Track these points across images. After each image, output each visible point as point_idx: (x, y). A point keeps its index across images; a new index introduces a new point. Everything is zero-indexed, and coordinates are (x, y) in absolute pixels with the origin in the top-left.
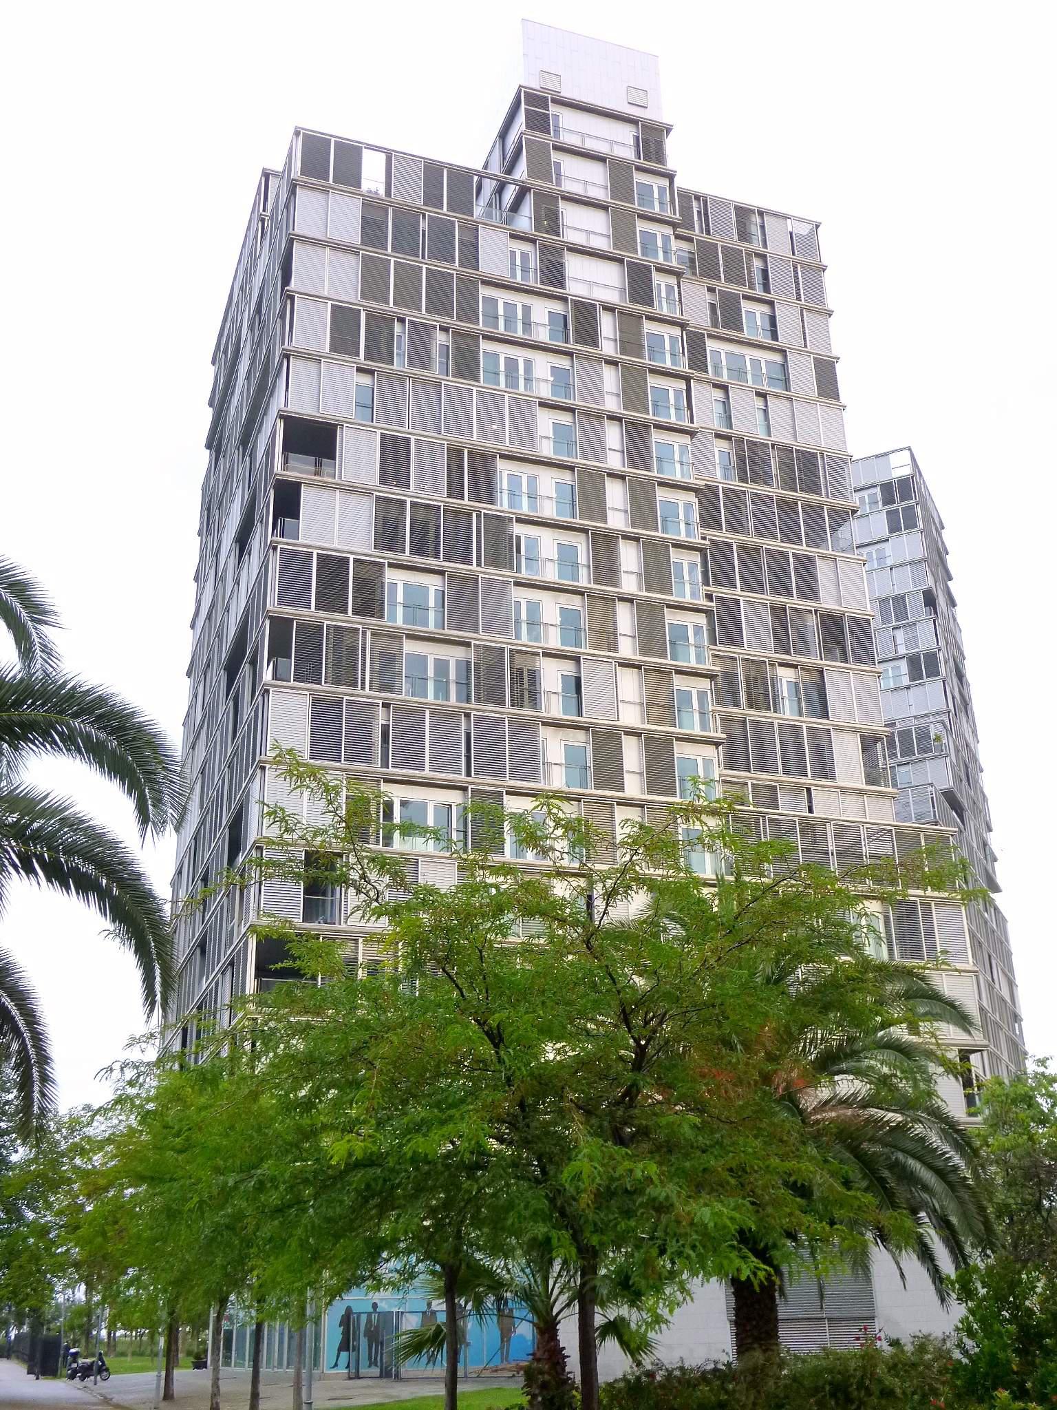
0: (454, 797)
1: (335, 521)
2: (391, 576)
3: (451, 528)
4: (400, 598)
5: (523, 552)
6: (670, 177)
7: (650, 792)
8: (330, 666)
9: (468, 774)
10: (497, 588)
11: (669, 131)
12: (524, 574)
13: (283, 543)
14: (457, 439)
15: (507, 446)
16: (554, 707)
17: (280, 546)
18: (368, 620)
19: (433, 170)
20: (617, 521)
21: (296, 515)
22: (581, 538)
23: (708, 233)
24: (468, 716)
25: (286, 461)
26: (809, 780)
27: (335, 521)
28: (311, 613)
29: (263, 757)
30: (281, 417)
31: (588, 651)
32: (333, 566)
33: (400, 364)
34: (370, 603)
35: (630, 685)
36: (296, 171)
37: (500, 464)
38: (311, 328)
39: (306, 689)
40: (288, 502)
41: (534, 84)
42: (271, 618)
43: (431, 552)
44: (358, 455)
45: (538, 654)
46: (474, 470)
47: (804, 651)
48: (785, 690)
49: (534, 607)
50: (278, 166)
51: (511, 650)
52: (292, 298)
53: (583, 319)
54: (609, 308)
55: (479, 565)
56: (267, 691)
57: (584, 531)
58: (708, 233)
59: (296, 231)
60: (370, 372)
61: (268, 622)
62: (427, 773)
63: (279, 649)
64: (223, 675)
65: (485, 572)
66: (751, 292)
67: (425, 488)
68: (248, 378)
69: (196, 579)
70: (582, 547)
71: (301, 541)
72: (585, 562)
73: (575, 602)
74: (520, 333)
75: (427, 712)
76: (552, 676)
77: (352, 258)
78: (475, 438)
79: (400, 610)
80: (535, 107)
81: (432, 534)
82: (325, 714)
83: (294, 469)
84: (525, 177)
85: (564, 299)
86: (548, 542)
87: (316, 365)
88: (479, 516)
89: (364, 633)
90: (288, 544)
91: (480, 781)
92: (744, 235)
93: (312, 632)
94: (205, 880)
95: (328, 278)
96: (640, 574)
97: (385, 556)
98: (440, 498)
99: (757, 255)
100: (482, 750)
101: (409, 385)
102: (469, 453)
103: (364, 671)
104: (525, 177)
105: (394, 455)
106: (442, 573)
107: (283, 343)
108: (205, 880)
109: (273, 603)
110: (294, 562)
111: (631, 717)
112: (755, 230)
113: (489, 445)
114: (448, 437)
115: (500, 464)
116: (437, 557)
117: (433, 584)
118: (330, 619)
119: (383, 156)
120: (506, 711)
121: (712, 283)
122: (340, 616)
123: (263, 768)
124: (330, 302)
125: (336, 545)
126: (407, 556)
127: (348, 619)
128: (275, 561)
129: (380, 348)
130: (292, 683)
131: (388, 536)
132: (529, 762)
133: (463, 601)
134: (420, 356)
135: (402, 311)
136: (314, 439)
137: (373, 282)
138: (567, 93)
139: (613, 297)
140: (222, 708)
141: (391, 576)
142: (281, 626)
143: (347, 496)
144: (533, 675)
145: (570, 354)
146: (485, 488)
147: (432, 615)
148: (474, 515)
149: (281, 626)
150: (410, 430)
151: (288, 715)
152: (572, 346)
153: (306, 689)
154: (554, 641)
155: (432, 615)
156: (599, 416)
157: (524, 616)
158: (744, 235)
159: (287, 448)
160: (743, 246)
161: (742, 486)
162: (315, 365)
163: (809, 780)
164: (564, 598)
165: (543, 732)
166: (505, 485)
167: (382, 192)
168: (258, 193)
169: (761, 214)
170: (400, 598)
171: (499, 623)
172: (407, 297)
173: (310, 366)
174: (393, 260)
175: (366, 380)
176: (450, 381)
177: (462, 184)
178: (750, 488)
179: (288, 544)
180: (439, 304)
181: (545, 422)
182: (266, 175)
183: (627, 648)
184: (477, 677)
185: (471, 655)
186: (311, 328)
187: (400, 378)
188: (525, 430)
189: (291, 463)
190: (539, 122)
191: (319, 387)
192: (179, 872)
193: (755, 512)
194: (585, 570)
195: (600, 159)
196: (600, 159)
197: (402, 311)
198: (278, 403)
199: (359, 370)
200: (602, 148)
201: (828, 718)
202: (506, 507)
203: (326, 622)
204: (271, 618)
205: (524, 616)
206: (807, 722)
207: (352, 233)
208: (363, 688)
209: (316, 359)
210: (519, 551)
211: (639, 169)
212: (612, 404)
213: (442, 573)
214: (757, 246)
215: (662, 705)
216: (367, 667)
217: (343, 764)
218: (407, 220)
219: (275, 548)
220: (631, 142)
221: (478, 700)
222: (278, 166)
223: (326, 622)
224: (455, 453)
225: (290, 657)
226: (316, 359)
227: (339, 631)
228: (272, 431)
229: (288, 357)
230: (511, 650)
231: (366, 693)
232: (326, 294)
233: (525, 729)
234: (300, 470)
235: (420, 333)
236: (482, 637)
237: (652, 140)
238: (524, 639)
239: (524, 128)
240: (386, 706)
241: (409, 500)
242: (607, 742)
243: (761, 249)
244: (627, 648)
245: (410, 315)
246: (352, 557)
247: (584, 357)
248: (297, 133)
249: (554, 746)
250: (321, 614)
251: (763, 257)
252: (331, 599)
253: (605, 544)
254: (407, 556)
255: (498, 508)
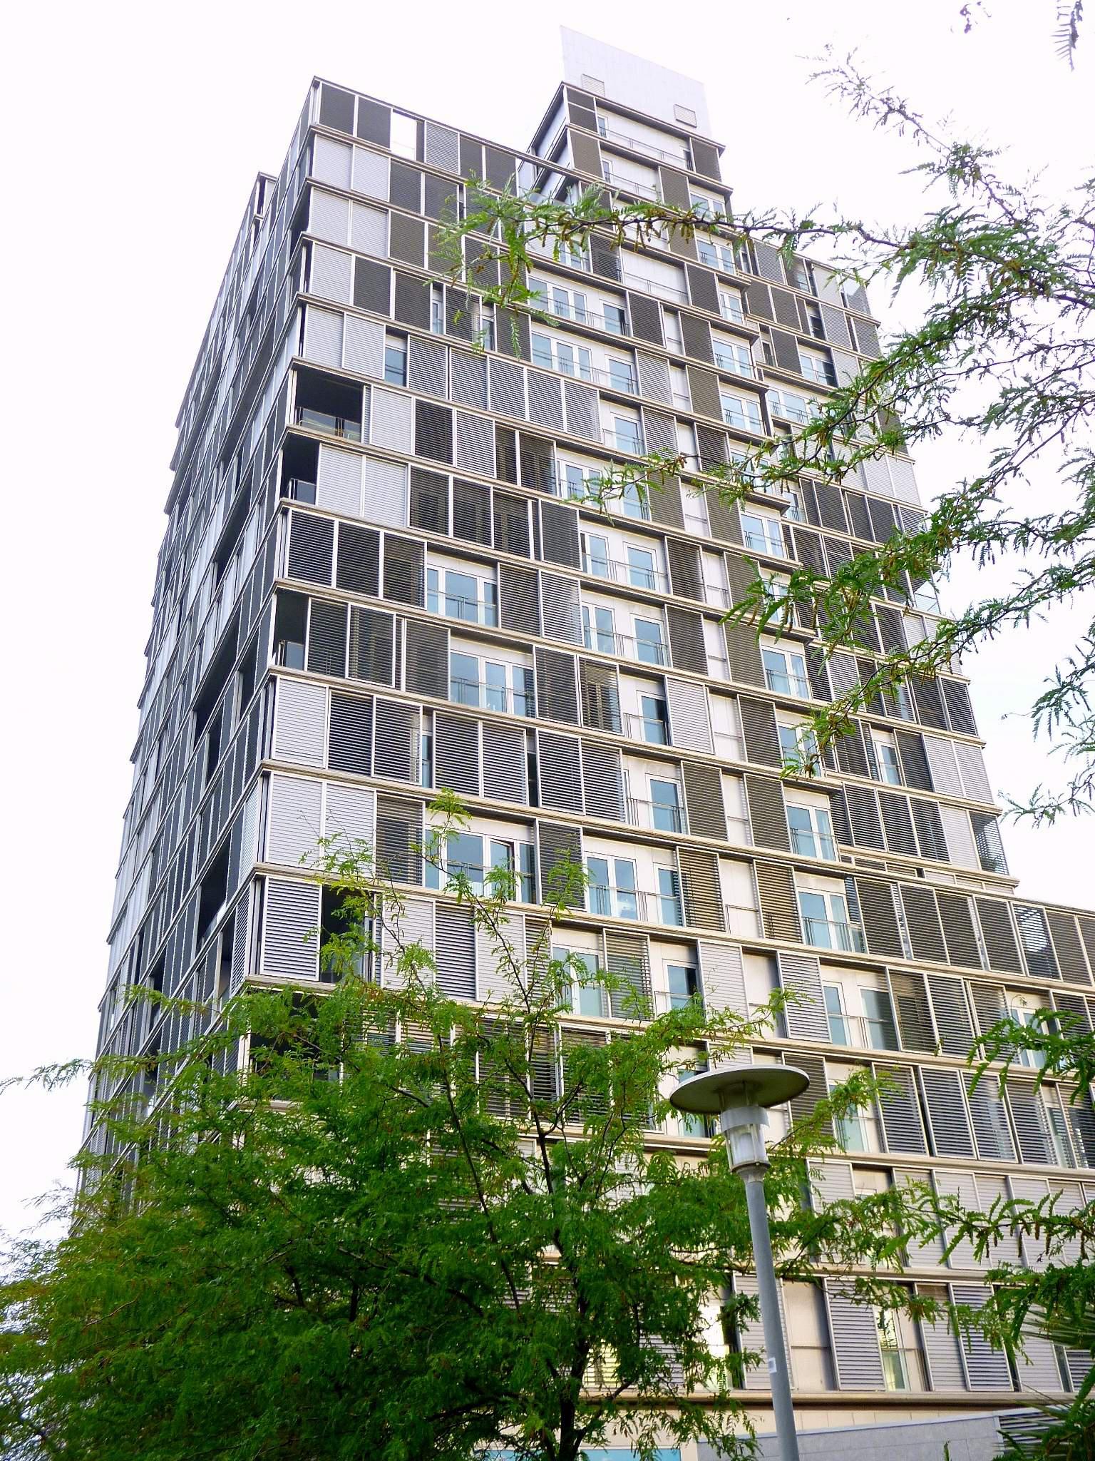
0: (517, 834)
1: (361, 488)
2: (431, 561)
3: (502, 508)
4: (442, 587)
5: (588, 551)
6: (726, 194)
7: (757, 844)
8: (356, 649)
9: (534, 802)
10: (559, 587)
11: (721, 150)
12: (591, 574)
13: (295, 506)
14: (509, 419)
15: (565, 432)
16: (638, 732)
17: (291, 509)
18: (403, 606)
19: (471, 145)
20: (695, 527)
21: (312, 478)
22: (653, 546)
23: (756, 273)
24: (531, 732)
25: (299, 417)
26: (919, 859)
27: (361, 488)
28: (332, 590)
29: (266, 761)
30: (294, 369)
31: (672, 669)
32: (359, 542)
33: (437, 328)
34: (406, 586)
35: (724, 715)
36: (315, 118)
37: (558, 455)
38: (332, 277)
39: (326, 681)
40: (301, 462)
41: (576, 82)
42: (280, 593)
43: (479, 532)
44: (390, 419)
45: (613, 668)
46: (530, 456)
47: (895, 713)
48: (881, 756)
49: (604, 614)
50: (275, 171)
51: (581, 659)
52: (308, 246)
53: (644, 315)
54: (672, 310)
55: (538, 557)
56: (273, 679)
57: (660, 536)
58: (756, 273)
59: (314, 176)
60: (402, 335)
61: (274, 598)
62: (481, 798)
63: (289, 629)
64: (192, 718)
65: (546, 567)
66: (805, 337)
67: (473, 466)
68: (234, 385)
69: (147, 653)
70: (657, 557)
71: (317, 505)
72: (661, 570)
73: (653, 614)
74: (572, 317)
75: (480, 724)
76: (632, 697)
77: (377, 217)
78: (526, 420)
79: (442, 601)
80: (580, 105)
81: (479, 522)
82: (349, 719)
83: (308, 425)
84: (572, 167)
85: (620, 293)
86: (617, 545)
87: (337, 319)
88: (535, 505)
89: (399, 622)
90: (302, 507)
91: (545, 813)
92: (793, 282)
93: (332, 615)
94: (157, 976)
95: (350, 234)
96: (725, 592)
97: (425, 536)
98: (489, 479)
99: (810, 303)
100: (549, 774)
101: (448, 357)
102: (521, 435)
103: (399, 660)
104: (572, 167)
105: (433, 429)
106: (492, 563)
107: (296, 287)
108: (157, 976)
109: (281, 572)
110: (311, 534)
111: (728, 751)
112: (802, 278)
113: (544, 429)
114: (493, 416)
115: (558, 455)
116: (487, 542)
117: (483, 575)
118: (355, 600)
119: (414, 123)
120: (578, 730)
121: (766, 322)
122: (371, 599)
123: (266, 776)
124: (354, 255)
125: (362, 516)
126: (449, 538)
127: (379, 602)
128: (284, 530)
129: (413, 302)
130: (306, 672)
131: (426, 509)
132: (607, 797)
133: (521, 600)
134: (461, 327)
135: (437, 276)
136: (335, 397)
137: (405, 239)
138: (613, 96)
139: (675, 299)
140: (189, 753)
141: (431, 561)
142: (292, 604)
143: (376, 464)
144: (607, 694)
145: (630, 349)
146: (540, 475)
147: (481, 611)
148: (530, 502)
149: (292, 604)
150: (450, 401)
151: (299, 710)
152: (631, 338)
153: (326, 681)
154: (631, 654)
155: (481, 611)
156: (666, 416)
157: (593, 624)
158: (793, 282)
159: (301, 402)
160: (793, 291)
161: (813, 529)
162: (335, 319)
163: (919, 859)
164: (639, 608)
165: (625, 762)
166: (564, 477)
167: (412, 156)
168: (251, 204)
169: (809, 264)
170: (442, 587)
171: (562, 628)
172: (445, 262)
173: (331, 320)
174: (427, 224)
175: (397, 344)
176: (494, 355)
177: (503, 160)
178: (823, 532)
179: (302, 507)
180: (481, 273)
181: (607, 416)
182: (262, 180)
183: (717, 672)
184: (541, 686)
185: (532, 663)
186: (332, 277)
187: (437, 345)
188: (583, 419)
189: (306, 420)
190: (584, 118)
191: (343, 342)
192: (113, 988)
193: (831, 557)
194: (662, 581)
195: (653, 166)
196: (653, 166)
197: (437, 276)
198: (291, 350)
199: (390, 331)
200: (654, 155)
201: (931, 789)
202: (565, 496)
203: (350, 603)
204: (280, 593)
205: (593, 624)
206: (910, 793)
207: (382, 192)
208: (398, 687)
209: (338, 312)
210: (584, 550)
211: (694, 182)
212: (680, 405)
213: (492, 563)
214: (805, 291)
215: (760, 739)
216: (402, 661)
217: (374, 778)
218: (441, 187)
219: (285, 512)
220: (683, 155)
221: (542, 714)
222: (275, 171)
223: (350, 603)
224: (505, 434)
225: (304, 643)
226: (338, 312)
227: (366, 617)
228: (283, 379)
229: (302, 305)
230: (581, 659)
231: (400, 693)
232: (349, 245)
233: (604, 756)
234: (316, 427)
235: (457, 300)
236: (544, 641)
237: (705, 156)
238: (595, 649)
239: (568, 121)
240: (428, 712)
241: (451, 477)
242: (703, 779)
243: (811, 297)
244: (717, 672)
245: (446, 280)
246: (382, 532)
247: (646, 353)
248: (315, 84)
249: (638, 780)
250: (345, 593)
251: (814, 305)
252: (357, 578)
253: (683, 556)
254: (449, 538)
255: (558, 497)
